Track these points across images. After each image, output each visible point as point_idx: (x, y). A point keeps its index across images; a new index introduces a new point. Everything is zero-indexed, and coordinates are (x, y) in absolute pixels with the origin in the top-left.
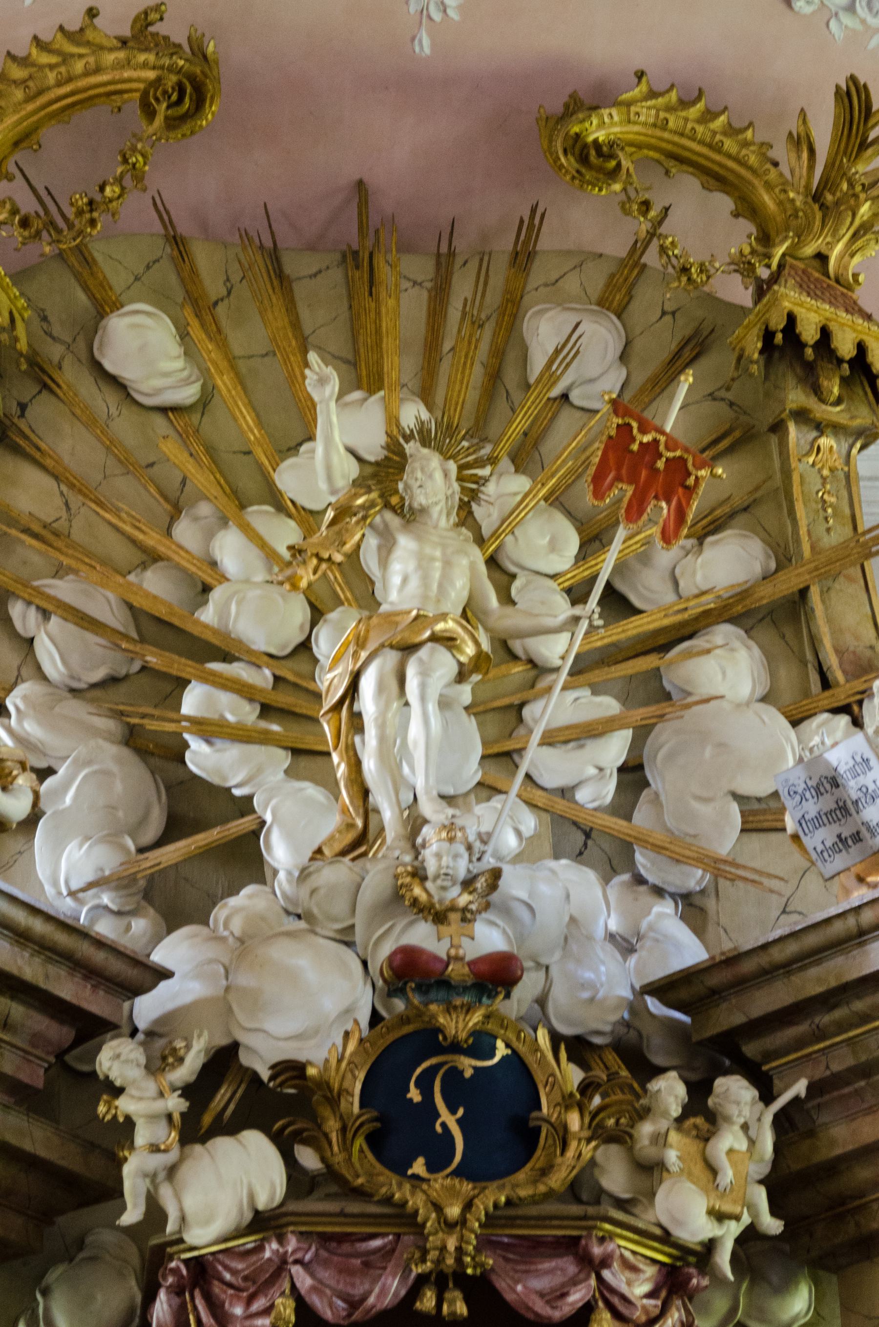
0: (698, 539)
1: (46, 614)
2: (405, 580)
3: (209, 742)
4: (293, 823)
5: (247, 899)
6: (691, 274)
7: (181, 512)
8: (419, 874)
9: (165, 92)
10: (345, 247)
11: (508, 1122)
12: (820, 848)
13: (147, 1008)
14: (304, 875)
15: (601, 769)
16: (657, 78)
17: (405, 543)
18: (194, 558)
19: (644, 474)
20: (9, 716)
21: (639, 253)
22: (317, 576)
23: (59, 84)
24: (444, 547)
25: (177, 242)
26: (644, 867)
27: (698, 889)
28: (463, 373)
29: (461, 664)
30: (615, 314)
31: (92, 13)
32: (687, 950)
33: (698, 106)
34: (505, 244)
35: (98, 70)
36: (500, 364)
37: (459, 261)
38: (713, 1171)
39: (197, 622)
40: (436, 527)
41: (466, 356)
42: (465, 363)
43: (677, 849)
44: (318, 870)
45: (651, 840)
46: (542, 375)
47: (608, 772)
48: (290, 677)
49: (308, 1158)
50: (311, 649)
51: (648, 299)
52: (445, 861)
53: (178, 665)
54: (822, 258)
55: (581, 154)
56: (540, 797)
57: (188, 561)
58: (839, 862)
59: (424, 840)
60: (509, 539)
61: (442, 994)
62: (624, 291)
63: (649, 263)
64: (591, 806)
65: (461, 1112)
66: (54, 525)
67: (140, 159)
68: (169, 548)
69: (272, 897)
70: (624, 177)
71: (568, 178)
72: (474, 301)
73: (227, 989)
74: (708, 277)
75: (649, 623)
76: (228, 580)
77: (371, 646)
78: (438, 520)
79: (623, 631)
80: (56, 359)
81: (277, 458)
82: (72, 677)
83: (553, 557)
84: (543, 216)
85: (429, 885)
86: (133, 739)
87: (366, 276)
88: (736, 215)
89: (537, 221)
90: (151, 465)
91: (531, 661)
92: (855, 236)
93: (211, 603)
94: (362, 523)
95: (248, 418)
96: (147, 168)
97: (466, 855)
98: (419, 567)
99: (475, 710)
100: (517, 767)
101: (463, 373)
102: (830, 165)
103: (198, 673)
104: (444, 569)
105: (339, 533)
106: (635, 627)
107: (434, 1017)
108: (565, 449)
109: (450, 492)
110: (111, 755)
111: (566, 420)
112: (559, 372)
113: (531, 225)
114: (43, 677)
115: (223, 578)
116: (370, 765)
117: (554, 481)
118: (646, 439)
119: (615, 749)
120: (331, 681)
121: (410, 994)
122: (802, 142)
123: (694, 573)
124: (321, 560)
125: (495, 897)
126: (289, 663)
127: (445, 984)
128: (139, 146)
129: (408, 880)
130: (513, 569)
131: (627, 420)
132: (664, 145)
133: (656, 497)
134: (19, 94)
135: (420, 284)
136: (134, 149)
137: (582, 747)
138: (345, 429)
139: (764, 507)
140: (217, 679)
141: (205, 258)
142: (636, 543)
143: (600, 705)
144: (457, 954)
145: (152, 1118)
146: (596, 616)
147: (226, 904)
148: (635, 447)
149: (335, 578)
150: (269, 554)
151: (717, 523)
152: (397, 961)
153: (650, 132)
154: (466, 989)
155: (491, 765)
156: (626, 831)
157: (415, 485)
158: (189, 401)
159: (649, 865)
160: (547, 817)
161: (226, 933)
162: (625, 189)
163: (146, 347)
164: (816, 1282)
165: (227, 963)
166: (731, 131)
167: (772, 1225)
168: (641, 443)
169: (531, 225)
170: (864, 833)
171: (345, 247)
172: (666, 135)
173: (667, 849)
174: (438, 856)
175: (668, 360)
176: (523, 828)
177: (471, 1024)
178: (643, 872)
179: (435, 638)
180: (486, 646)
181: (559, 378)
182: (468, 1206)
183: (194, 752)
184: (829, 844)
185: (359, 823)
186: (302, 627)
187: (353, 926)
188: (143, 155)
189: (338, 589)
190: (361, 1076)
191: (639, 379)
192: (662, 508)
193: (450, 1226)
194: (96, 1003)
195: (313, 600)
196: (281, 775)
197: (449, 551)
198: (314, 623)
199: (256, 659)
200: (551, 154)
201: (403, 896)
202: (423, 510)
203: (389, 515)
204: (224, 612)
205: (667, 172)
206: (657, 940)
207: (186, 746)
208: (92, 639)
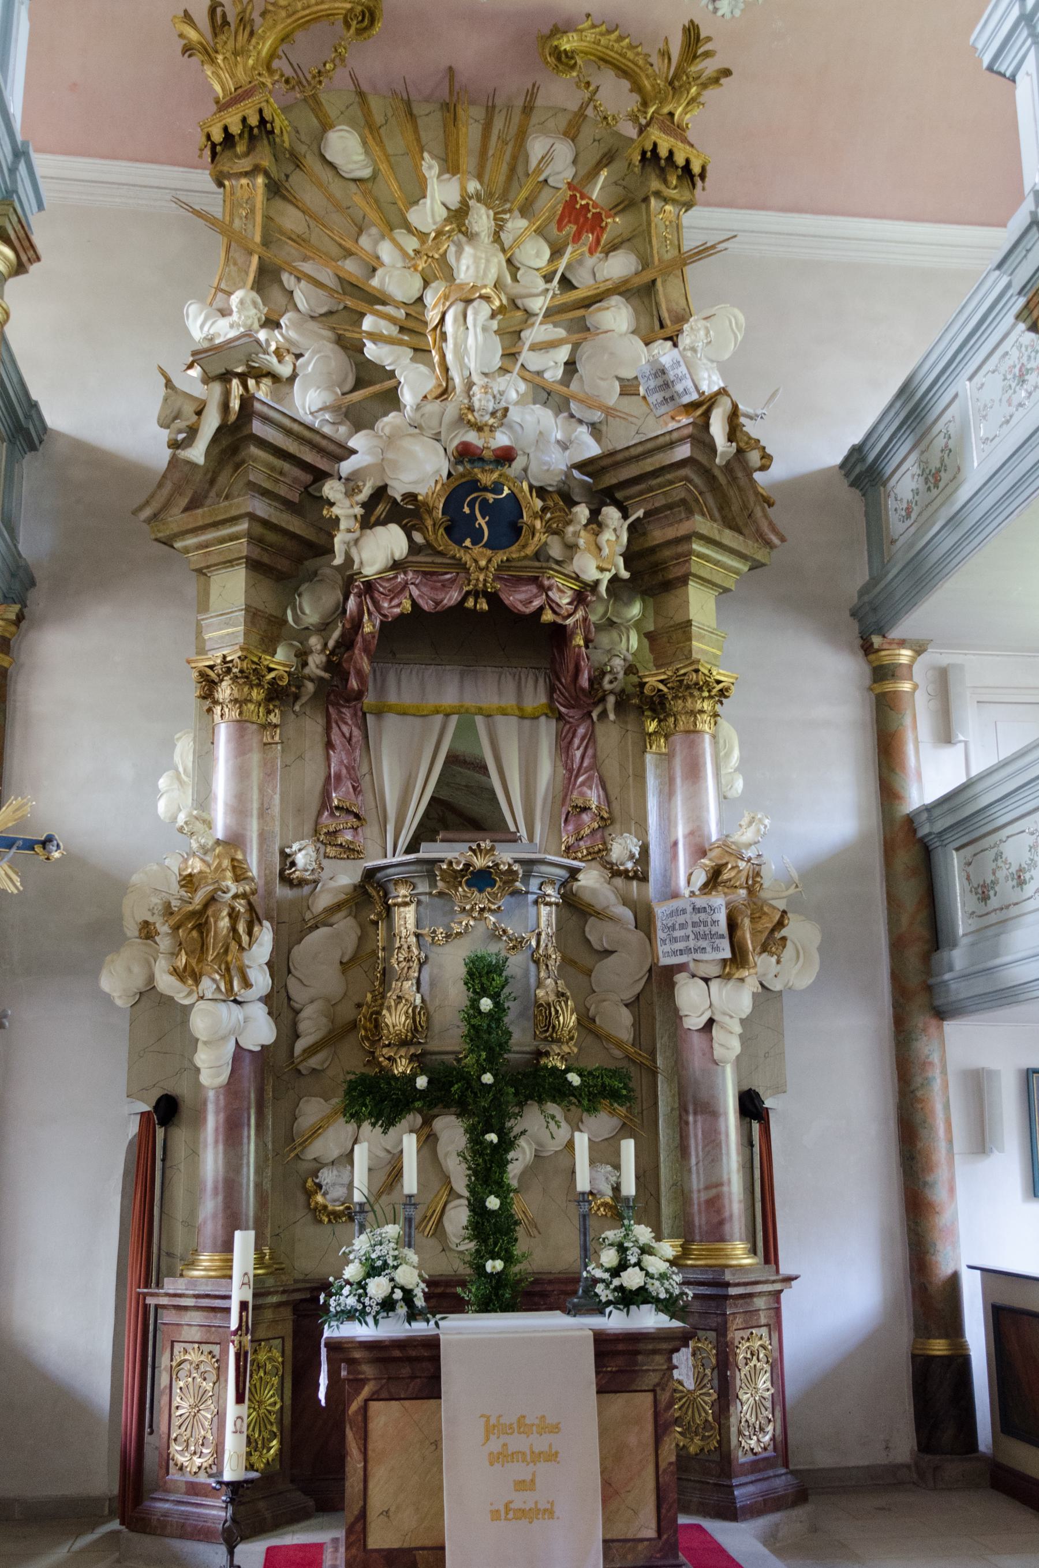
1: (299, 279)
2: (468, 268)
3: (375, 343)
4: (413, 383)
8: (471, 409)
13: (346, 467)
17: (468, 250)
19: (582, 220)
20: (281, 327)
23: (304, 9)
25: (361, 94)
32: (593, 449)
34: (519, 103)
37: (497, 110)
38: (600, 549)
48: (414, 314)
49: (418, 537)
51: (588, 132)
53: (361, 306)
54: (671, 114)
56: (527, 375)
58: (663, 409)
61: (480, 464)
65: (487, 518)
73: (383, 459)
77: (451, 300)
83: (538, 260)
85: (475, 414)
86: (340, 341)
88: (631, 91)
91: (525, 310)
92: (688, 104)
107: (476, 474)
110: (330, 349)
111: (546, 192)
114: (299, 311)
115: (383, 265)
116: (449, 357)
118: (584, 202)
119: (563, 354)
120: (432, 316)
122: (665, 54)
124: (428, 257)
125: (505, 420)
126: (412, 307)
127: (481, 459)
130: (519, 265)
134: (283, 14)
138: (441, 193)
139: (637, 239)
141: (374, 102)
145: (348, 517)
148: (578, 206)
150: (404, 253)
160: (531, 385)
163: (346, 147)
164: (644, 601)
166: (631, 47)
167: (625, 574)
172: (599, 48)
174: (480, 400)
179: (481, 297)
180: (505, 302)
182: (489, 561)
185: (444, 384)
190: (443, 500)
191: (582, 172)
193: (481, 569)
194: (322, 464)
196: (408, 360)
198: (424, 288)
199: (398, 304)
203: (461, 236)
205: (599, 68)
207: (365, 345)
208: (320, 292)
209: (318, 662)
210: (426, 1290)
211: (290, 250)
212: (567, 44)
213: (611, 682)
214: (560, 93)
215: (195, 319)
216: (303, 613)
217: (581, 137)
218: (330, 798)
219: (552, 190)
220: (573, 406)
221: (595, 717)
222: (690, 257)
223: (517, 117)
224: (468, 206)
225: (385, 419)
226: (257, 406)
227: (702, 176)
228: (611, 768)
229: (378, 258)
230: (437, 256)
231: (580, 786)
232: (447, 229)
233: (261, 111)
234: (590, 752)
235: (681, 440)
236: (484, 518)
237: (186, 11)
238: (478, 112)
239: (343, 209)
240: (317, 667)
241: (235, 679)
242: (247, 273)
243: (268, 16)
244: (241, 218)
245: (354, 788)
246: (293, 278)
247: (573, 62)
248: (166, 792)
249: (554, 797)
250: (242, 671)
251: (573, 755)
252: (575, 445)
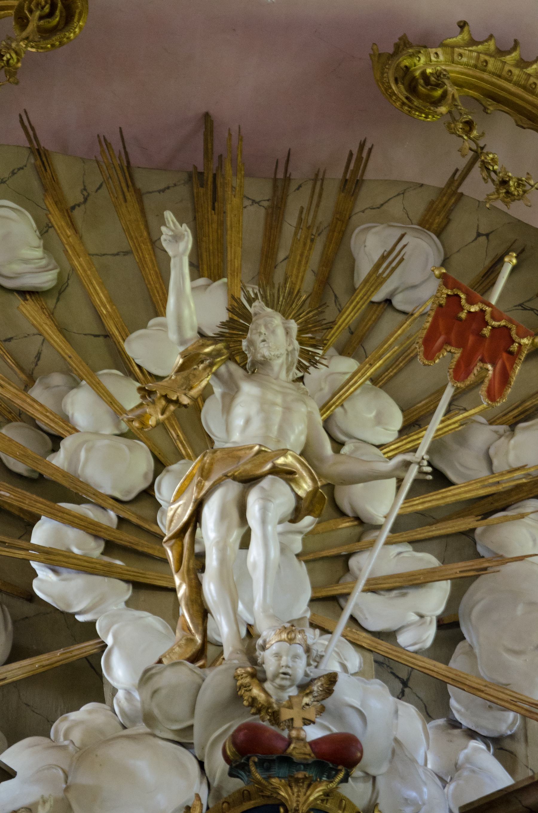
0: (510, 426)
2: (248, 421)
3: (55, 571)
4: (131, 646)
5: (88, 713)
6: (509, 186)
7: (35, 382)
8: (258, 676)
9: (38, 4)
10: (191, 169)
14: (146, 677)
15: (422, 616)
16: (477, 29)
17: (249, 390)
18: (47, 411)
19: (471, 339)
21: (456, 184)
22: (165, 416)
24: (285, 395)
25: (40, 155)
26: (458, 711)
27: (509, 733)
28: (298, 269)
29: (298, 498)
30: (435, 234)
33: (513, 55)
34: (337, 174)
36: (330, 271)
37: (293, 186)
39: (49, 465)
40: (277, 378)
41: (302, 255)
42: (300, 261)
43: (492, 692)
44: (160, 673)
45: (468, 682)
46: (370, 275)
47: (428, 619)
48: (134, 519)
50: (153, 497)
51: (463, 224)
52: (284, 662)
53: (28, 500)
55: (410, 85)
56: (365, 639)
57: (41, 413)
59: (265, 641)
60: (339, 411)
61: (284, 771)
62: (443, 215)
63: (466, 193)
64: (411, 649)
67: (14, 56)
68: (25, 401)
69: (111, 713)
70: (450, 101)
71: (398, 104)
72: (309, 210)
73: (67, 789)
74: (524, 192)
75: (466, 492)
76: (77, 431)
77: (214, 477)
78: (279, 372)
79: (443, 498)
81: (127, 330)
83: (379, 429)
84: (370, 150)
85: (268, 686)
87: (210, 193)
89: (364, 155)
90: (9, 340)
91: (357, 518)
93: (62, 450)
94: (208, 370)
95: (102, 295)
96: (19, 65)
97: (304, 657)
98: (262, 410)
99: (306, 558)
100: (342, 609)
101: (298, 269)
103: (48, 509)
104: (284, 413)
105: (187, 379)
106: (454, 495)
107: (275, 790)
108: (392, 335)
109: (290, 348)
111: (389, 320)
112: (385, 275)
116: (211, 589)
117: (381, 362)
119: (434, 599)
120: (174, 511)
121: (253, 769)
123: (507, 453)
124: (169, 401)
125: (328, 702)
126: (133, 508)
127: (287, 760)
128: (14, 45)
129: (248, 680)
131: (456, 291)
132: (483, 85)
133: (482, 361)
135: (258, 203)
136: (8, 48)
137: (404, 595)
138: (193, 306)
140: (66, 516)
141: (64, 170)
142: (454, 423)
143: (421, 559)
144: (298, 735)
146: (425, 463)
147: (66, 718)
148: (463, 315)
149: (178, 436)
150: (117, 409)
151: (528, 413)
152: (241, 736)
153: (471, 72)
154: (307, 766)
155: (319, 607)
156: (444, 673)
157: (258, 339)
158: (48, 286)
159: (463, 710)
160: (370, 657)
161: (66, 743)
162: (450, 112)
165: (66, 768)
168: (469, 312)
171: (191, 169)
172: (485, 76)
173: (482, 691)
174: (278, 656)
175: (482, 274)
176: (349, 665)
177: (311, 798)
178: (458, 717)
179: (276, 471)
181: (385, 280)
183: (42, 580)
185: (198, 639)
186: (145, 475)
187: (191, 727)
188: (17, 53)
189: (180, 446)
192: (488, 370)
195: (156, 453)
196: (123, 605)
198: (157, 473)
200: (383, 83)
201: (242, 696)
202: (265, 363)
203: (233, 367)
204: (73, 458)
205: (485, 109)
206: (473, 771)
207: (35, 575)
212: (424, 63)
214: (414, 157)
217: (452, 228)
220: (456, 706)
223: (331, 190)
224: (248, 317)
225: (73, 716)
229: (66, 419)
230: (185, 400)
238: (261, 190)
247: (439, 92)
252: (466, 773)
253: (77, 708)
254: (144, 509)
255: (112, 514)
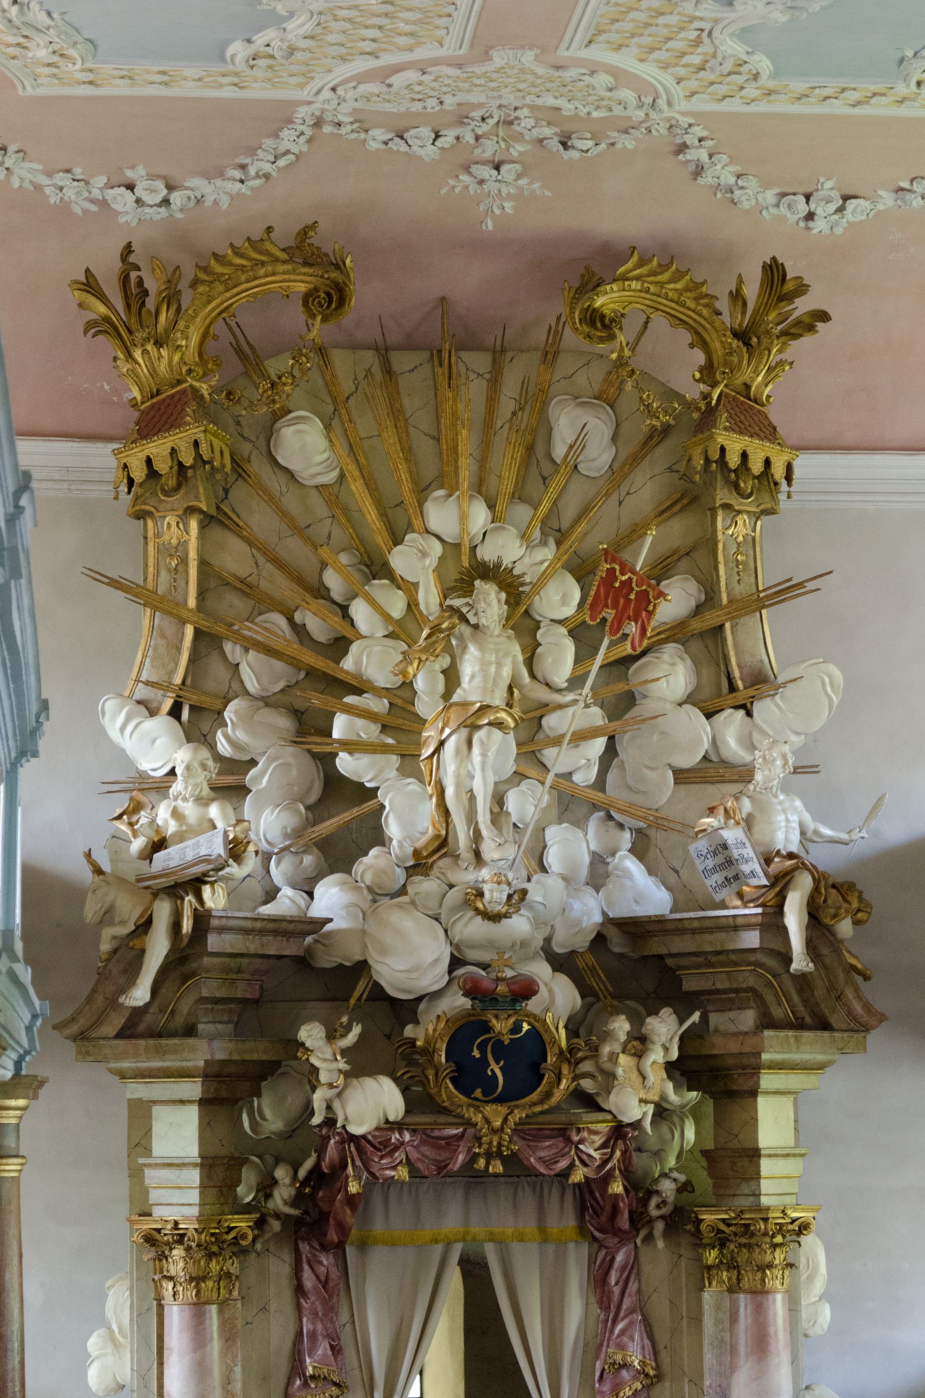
2: (473, 677)
4: (406, 818)
8: (480, 894)
11: (528, 1060)
12: (714, 885)
17: (473, 650)
19: (622, 601)
20: (226, 726)
23: (248, 281)
31: (269, 230)
35: (274, 274)
39: (342, 670)
54: (747, 387)
65: (502, 1063)
66: (249, 579)
80: (246, 455)
82: (263, 690)
87: (446, 371)
88: (692, 346)
89: (560, 329)
98: (482, 670)
102: (756, 311)
113: (556, 332)
114: (248, 693)
118: (624, 578)
122: (737, 297)
130: (539, 618)
137: (577, 746)
148: (617, 585)
150: (386, 617)
163: (306, 446)
169: (556, 332)
170: (741, 875)
182: (505, 1120)
184: (719, 883)
185: (444, 833)
190: (446, 1040)
191: (625, 453)
193: (494, 1131)
196: (394, 773)
197: (501, 654)
199: (380, 692)
204: (358, 663)
209: (286, 1196)
210: (122, 220)
211: (233, 604)
213: (658, 1207)
215: (114, 716)
216: (264, 1118)
218: (302, 1362)
219: (583, 479)
221: (638, 1241)
222: (768, 597)
225: (365, 860)
226: (214, 913)
227: (789, 478)
228: (660, 1308)
231: (619, 1336)
232: (444, 626)
233: (196, 444)
234: (633, 1287)
235: (749, 926)
236: (498, 1063)
237: (87, 271)
238: (479, 362)
239: (301, 531)
240: (286, 1203)
241: (188, 1249)
242: (179, 650)
243: (201, 289)
244: (169, 570)
245: (332, 1348)
246: (238, 648)
248: (98, 1357)
249: (586, 1345)
250: (199, 1245)
251: (611, 1292)
253: (366, 854)
254: (407, 694)
255: (386, 701)
